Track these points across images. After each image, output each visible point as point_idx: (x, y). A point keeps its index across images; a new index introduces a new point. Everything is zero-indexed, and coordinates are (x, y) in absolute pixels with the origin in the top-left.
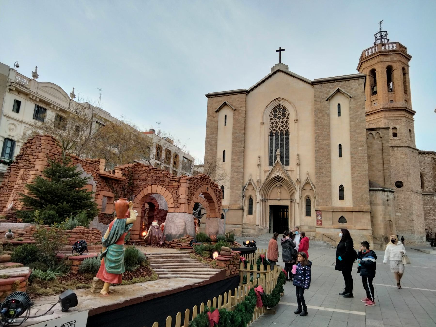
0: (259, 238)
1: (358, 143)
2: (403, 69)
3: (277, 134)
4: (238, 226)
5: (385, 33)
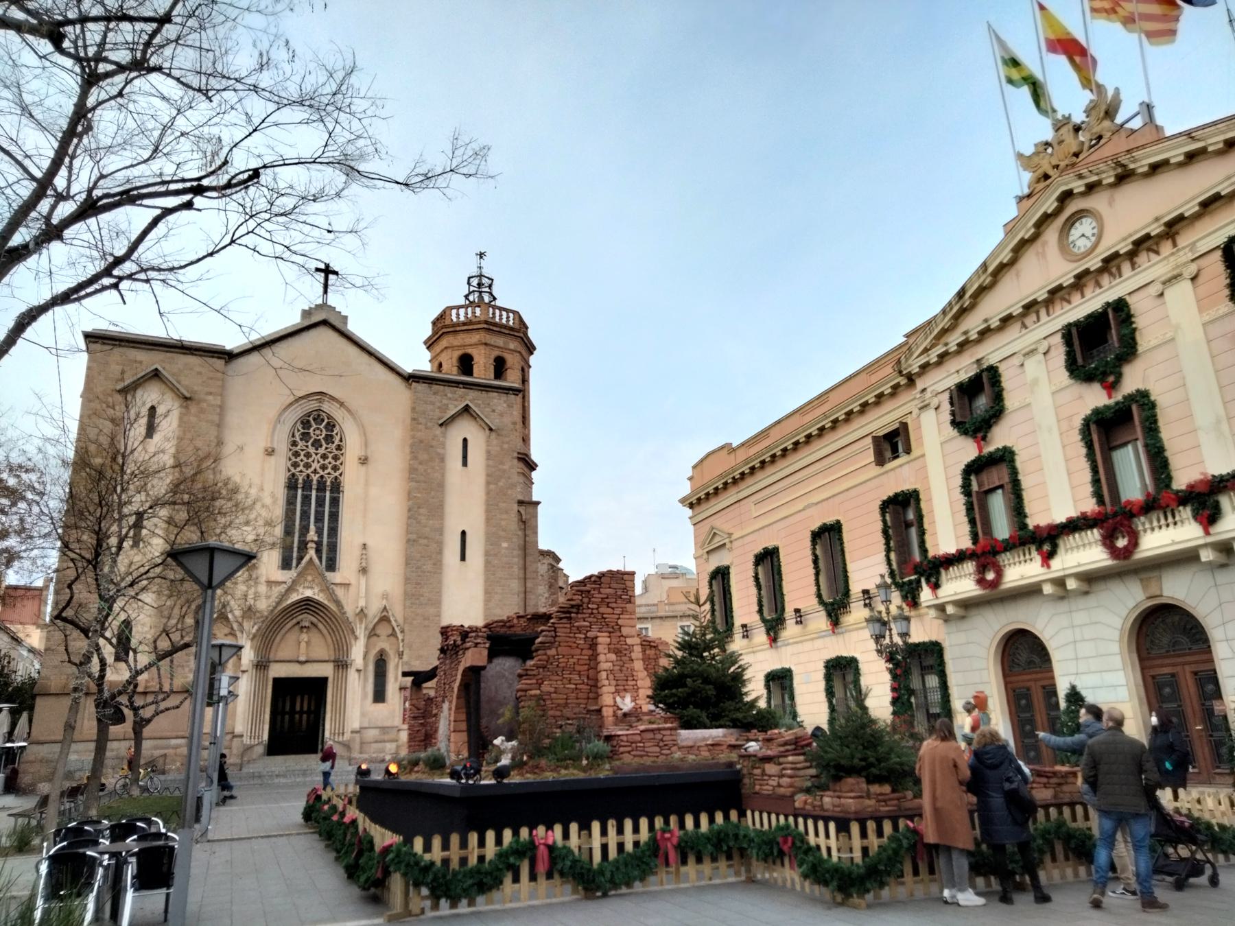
0: (245, 770)
1: (502, 533)
2: (523, 370)
3: (307, 484)
4: (173, 742)
5: (490, 282)
